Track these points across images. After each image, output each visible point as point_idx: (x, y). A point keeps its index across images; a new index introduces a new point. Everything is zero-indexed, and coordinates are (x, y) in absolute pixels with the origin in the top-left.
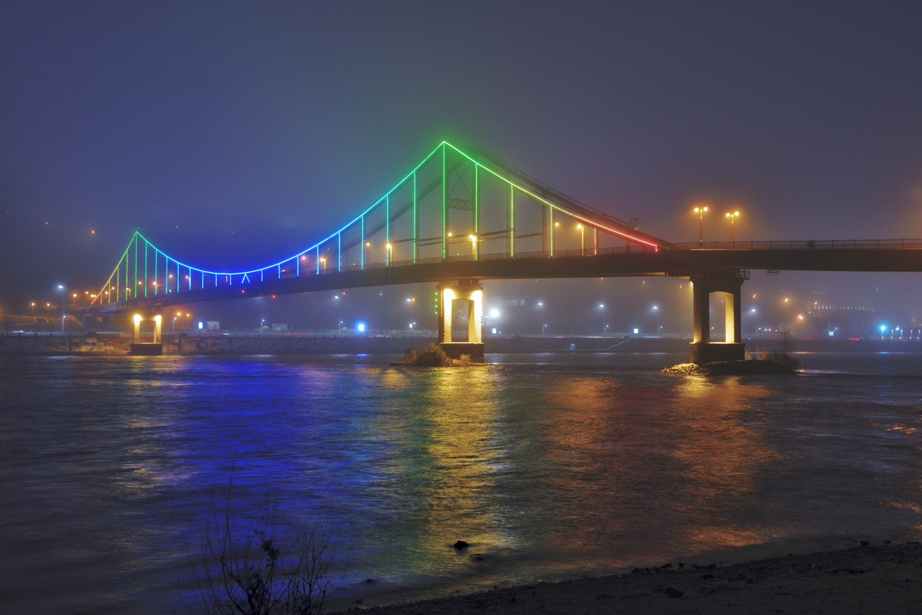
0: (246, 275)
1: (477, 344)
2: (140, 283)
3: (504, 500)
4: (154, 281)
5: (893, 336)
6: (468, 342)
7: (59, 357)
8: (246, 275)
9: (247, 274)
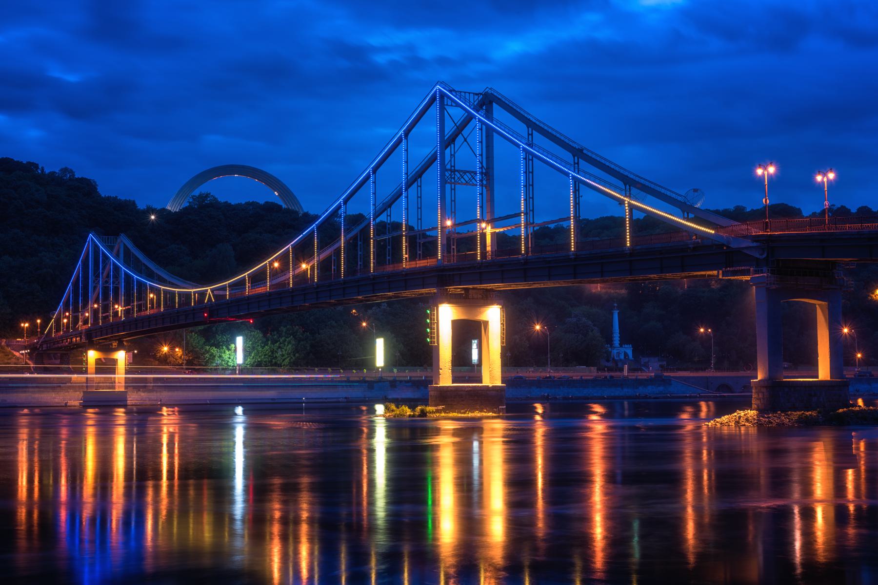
0: (209, 290)
1: (493, 386)
2: (96, 306)
3: (284, 538)
4: (308, 263)
5: (134, 350)
6: (482, 383)
7: (36, 490)
8: (209, 290)
9: (211, 289)
